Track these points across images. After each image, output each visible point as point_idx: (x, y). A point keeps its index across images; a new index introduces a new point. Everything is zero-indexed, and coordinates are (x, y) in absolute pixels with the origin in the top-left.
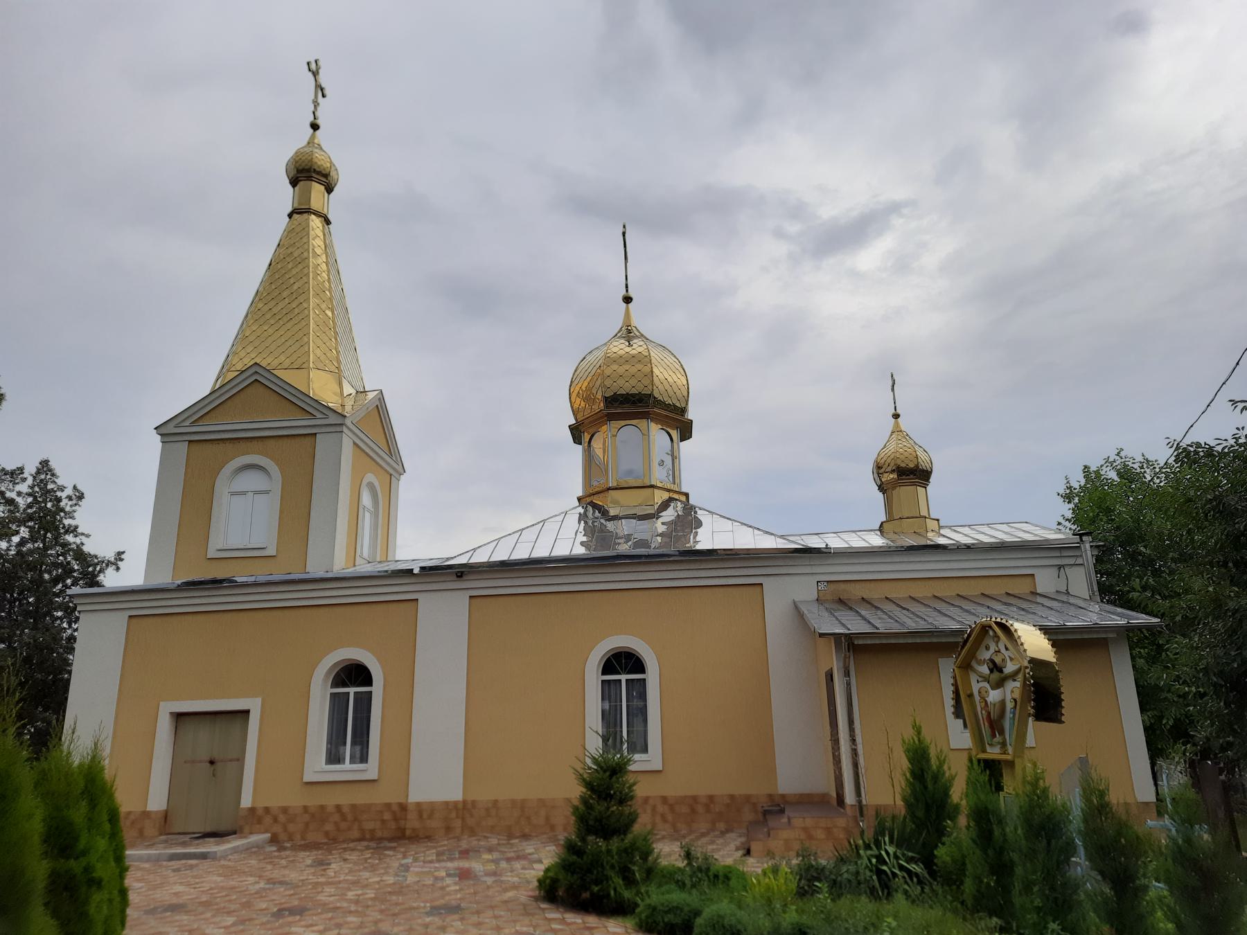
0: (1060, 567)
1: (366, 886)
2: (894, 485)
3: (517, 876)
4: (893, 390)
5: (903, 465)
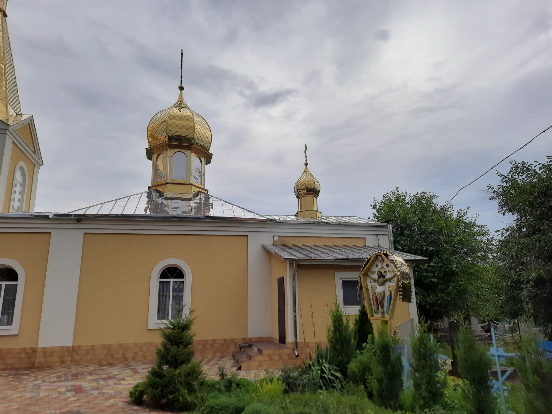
0: (377, 235)
1: (11, 401)
2: (305, 195)
3: (112, 389)
4: (305, 152)
5: (309, 187)
